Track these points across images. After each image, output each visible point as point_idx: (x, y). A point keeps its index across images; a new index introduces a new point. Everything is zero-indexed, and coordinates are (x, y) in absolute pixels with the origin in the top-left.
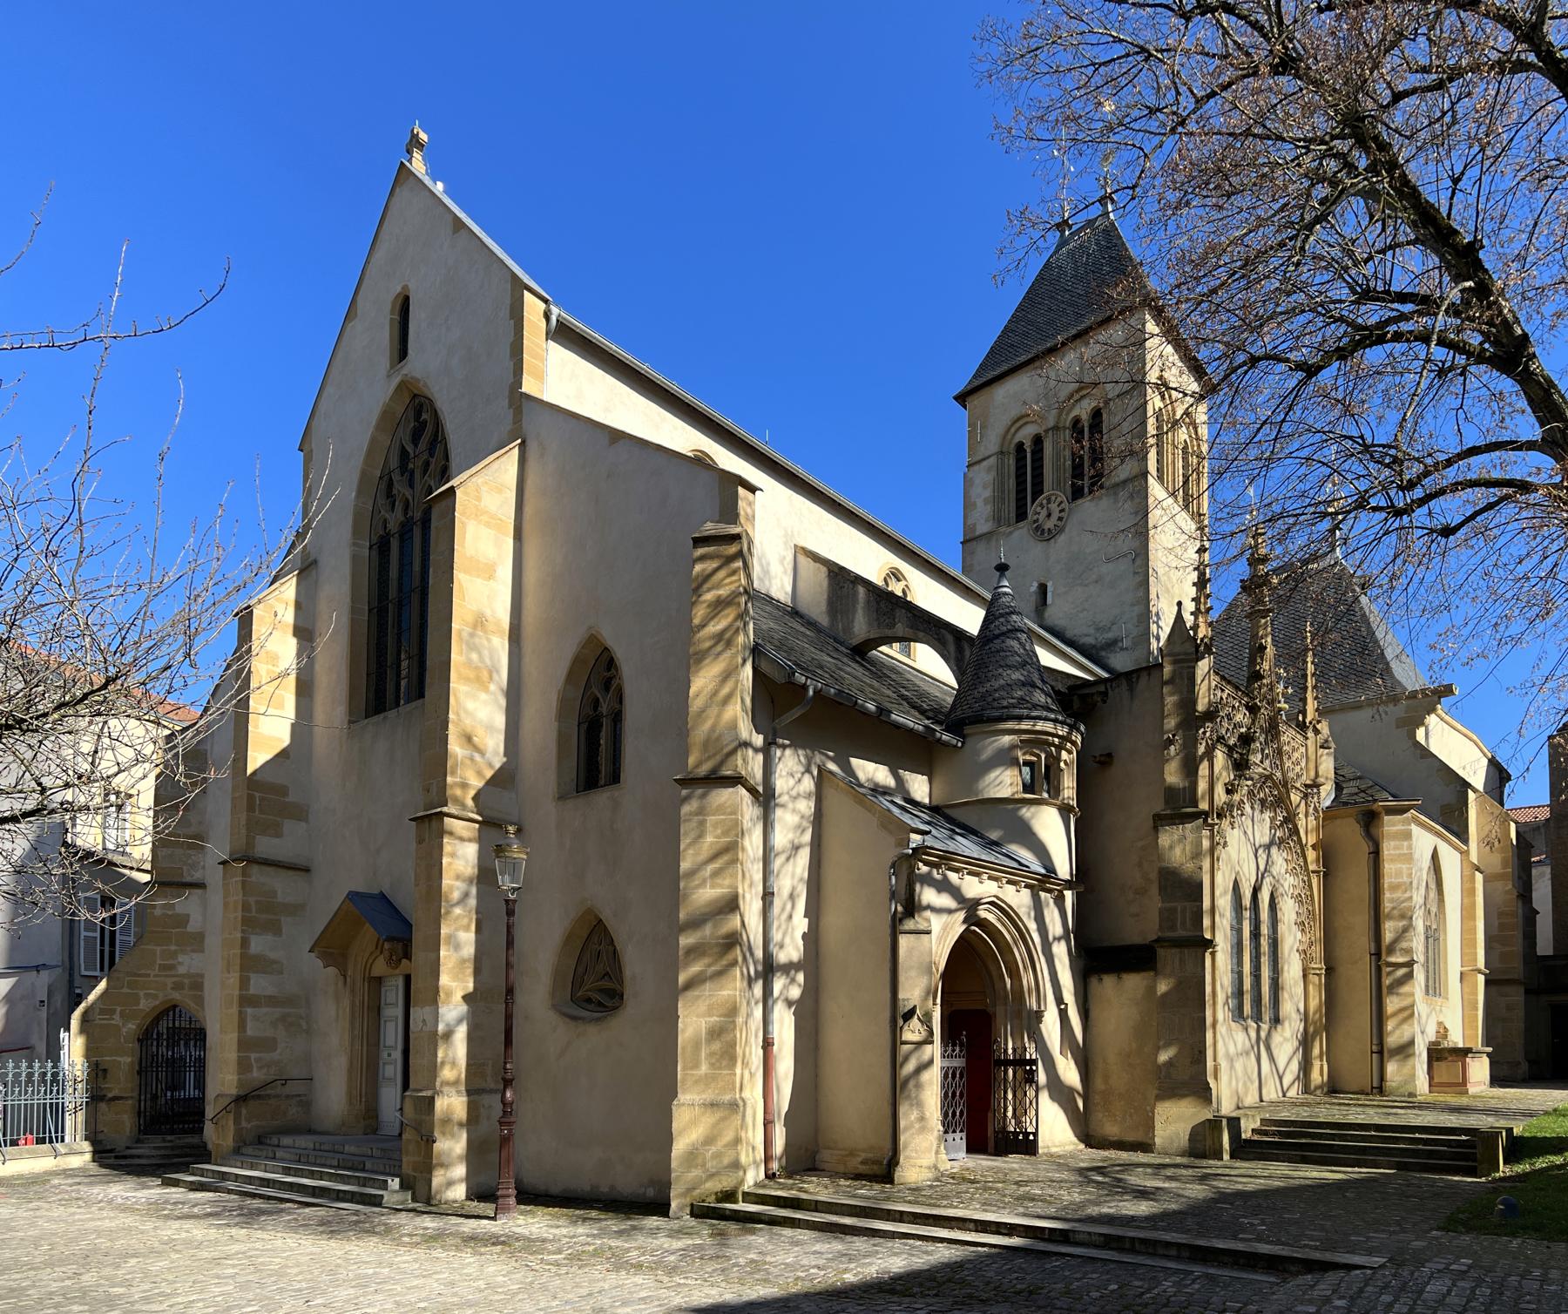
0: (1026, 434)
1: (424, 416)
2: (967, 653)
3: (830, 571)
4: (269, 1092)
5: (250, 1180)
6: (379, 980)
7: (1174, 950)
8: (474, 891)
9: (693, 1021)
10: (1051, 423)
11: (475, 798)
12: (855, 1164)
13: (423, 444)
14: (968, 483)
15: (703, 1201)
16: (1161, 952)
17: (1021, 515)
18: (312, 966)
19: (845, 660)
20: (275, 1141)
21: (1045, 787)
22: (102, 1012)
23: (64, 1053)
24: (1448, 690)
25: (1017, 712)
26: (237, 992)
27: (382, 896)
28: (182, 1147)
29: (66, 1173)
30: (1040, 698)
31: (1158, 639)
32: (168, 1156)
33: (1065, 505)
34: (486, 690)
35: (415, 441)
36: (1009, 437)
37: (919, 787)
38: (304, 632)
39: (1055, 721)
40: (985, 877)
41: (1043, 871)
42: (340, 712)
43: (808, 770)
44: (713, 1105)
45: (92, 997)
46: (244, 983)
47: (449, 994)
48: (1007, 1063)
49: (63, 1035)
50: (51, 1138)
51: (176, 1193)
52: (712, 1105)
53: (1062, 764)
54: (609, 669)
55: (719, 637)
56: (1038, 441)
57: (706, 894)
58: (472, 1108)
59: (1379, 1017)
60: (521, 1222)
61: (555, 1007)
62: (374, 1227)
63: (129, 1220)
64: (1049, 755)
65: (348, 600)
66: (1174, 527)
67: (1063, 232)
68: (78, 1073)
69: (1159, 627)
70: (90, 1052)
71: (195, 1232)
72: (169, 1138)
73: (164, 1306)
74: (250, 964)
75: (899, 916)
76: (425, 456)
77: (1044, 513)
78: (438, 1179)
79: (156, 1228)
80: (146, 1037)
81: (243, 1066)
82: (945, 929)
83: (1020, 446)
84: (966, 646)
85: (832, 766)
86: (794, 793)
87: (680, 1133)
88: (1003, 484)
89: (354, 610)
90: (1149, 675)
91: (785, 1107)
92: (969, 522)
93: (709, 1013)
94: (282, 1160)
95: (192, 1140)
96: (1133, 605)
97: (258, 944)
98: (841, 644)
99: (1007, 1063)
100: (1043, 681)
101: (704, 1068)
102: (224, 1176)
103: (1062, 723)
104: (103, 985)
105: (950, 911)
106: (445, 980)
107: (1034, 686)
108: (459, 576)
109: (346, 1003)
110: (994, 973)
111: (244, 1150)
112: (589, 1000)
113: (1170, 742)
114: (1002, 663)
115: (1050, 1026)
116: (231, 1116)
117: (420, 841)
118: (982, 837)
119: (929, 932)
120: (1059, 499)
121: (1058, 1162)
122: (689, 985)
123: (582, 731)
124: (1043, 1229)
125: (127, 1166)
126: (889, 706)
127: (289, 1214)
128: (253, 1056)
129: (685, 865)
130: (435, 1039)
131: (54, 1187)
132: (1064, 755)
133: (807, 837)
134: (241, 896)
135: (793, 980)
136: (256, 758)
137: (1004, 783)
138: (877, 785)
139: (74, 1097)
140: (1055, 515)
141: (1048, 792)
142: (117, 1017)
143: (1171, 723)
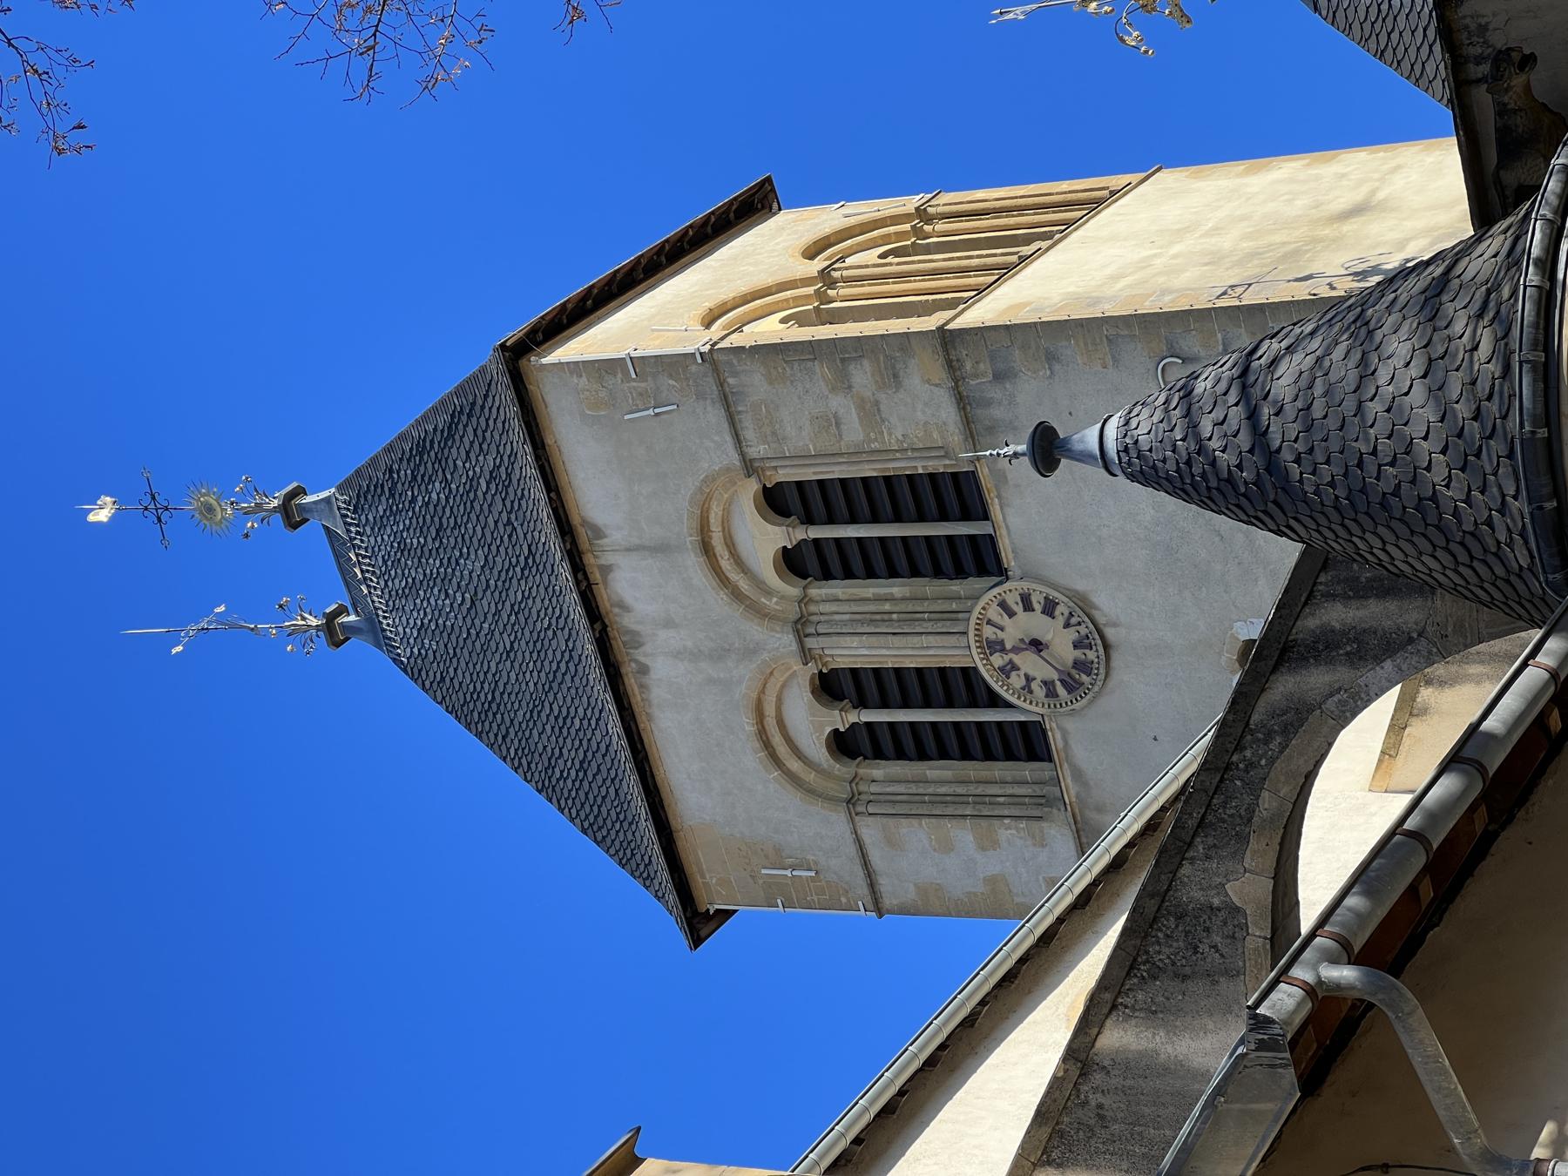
3: (1046, 1161)
10: (787, 641)
11: (853, 724)
25: (1527, 309)
33: (1010, 591)
36: (810, 777)
56: (830, 687)
67: (350, 630)
77: (1029, 663)
83: (843, 745)
88: (939, 799)
114: (1350, 405)
120: (994, 613)
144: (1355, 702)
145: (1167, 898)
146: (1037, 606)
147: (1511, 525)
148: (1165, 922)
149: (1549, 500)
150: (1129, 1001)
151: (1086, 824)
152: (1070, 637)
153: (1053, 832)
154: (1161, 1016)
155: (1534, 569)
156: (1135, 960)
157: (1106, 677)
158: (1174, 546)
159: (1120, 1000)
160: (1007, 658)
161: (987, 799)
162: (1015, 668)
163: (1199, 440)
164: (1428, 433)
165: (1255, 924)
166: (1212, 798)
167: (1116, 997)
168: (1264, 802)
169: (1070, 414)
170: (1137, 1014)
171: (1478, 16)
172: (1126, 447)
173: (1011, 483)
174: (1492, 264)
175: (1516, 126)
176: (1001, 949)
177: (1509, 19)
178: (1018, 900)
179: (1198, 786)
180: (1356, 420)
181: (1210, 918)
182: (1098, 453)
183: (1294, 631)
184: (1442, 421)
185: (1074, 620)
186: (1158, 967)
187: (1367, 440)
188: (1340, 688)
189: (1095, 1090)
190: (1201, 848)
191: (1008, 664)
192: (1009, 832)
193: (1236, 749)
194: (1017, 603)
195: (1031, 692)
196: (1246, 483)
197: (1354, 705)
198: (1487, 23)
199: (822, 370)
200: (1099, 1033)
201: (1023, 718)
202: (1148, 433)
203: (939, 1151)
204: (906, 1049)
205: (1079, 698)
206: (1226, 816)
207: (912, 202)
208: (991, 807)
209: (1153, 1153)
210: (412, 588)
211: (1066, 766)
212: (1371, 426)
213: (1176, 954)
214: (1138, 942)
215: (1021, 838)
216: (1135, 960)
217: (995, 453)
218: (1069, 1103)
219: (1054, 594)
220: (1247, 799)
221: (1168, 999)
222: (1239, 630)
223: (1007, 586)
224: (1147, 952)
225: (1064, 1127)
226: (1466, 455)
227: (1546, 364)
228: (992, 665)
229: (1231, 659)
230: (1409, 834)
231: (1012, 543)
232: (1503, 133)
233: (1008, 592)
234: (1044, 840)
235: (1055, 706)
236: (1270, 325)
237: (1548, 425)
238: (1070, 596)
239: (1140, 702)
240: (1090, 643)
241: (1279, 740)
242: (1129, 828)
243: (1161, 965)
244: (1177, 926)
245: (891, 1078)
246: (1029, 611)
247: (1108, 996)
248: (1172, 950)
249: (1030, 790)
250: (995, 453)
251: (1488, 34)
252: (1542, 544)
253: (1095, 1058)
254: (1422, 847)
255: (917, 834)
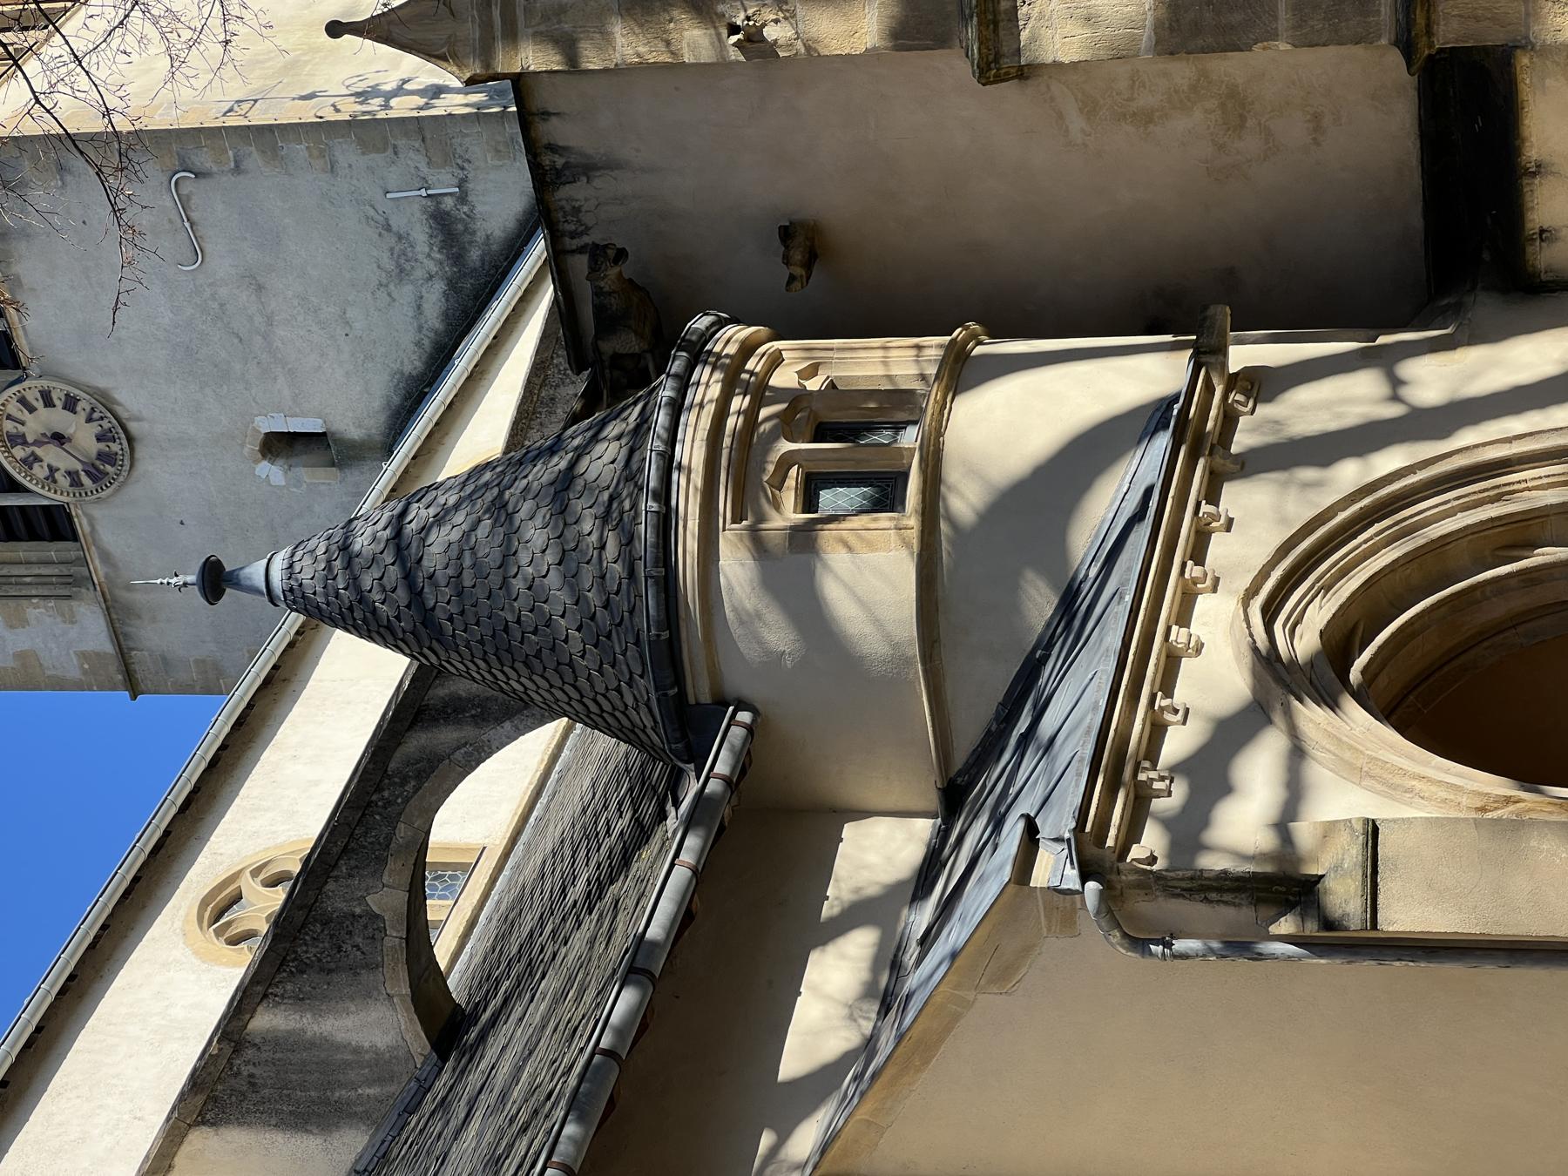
2: (462, 687)
3: (202, 1121)
16: (1449, 32)
19: (474, 1079)
21: (883, 437)
25: (645, 531)
30: (604, 460)
31: (437, 91)
39: (677, 408)
40: (1178, 635)
41: (1163, 441)
53: (813, 385)
66: (107, 53)
69: (399, 91)
75: (1311, 928)
82: (1361, 772)
84: (441, 692)
90: (546, 115)
92: (73, 672)
96: (332, 168)
98: (424, 1088)
100: (552, 451)
103: (684, 382)
105: (1297, 753)
107: (567, 478)
110: (1518, 602)
113: (753, 40)
114: (495, 580)
118: (1046, 644)
119: (1373, 831)
120: (14, 408)
126: (621, 941)
132: (784, 378)
138: (869, 991)
140: (58, 418)
141: (898, 427)
144: (479, 753)
145: (314, 908)
146: (57, 402)
147: (638, 696)
148: (312, 928)
149: (672, 688)
150: (279, 991)
151: (116, 601)
152: (94, 430)
153: (82, 610)
154: (308, 1001)
155: (657, 730)
156: (285, 958)
157: (132, 465)
158: (194, 347)
159: (270, 991)
160: (29, 450)
161: (13, 580)
162: (37, 459)
163: (359, 591)
164: (564, 612)
165: (393, 928)
166: (355, 829)
167: (267, 989)
168: (400, 833)
169: (84, 222)
170: (285, 1001)
171: (572, 200)
172: (291, 588)
173: (25, 287)
174: (611, 470)
175: (611, 305)
176: (116, 873)
177: (599, 205)
178: (48, 673)
179: (342, 821)
180: (501, 593)
181: (352, 924)
182: (265, 590)
183: (426, 698)
184: (576, 605)
185: (96, 415)
186: (306, 963)
187: (512, 610)
188: (466, 743)
189: (247, 1063)
190: (344, 869)
191: (30, 456)
192: (37, 610)
193: (375, 791)
194: (37, 400)
195: (55, 481)
196: (404, 632)
197: (478, 757)
198: (581, 206)
200: (251, 1017)
201: (46, 503)
202: (312, 579)
203: (79, 1083)
204: (39, 988)
205: (104, 488)
206: (366, 844)
208: (18, 587)
209: (299, 1110)
211: (93, 549)
212: (515, 600)
213: (322, 953)
214: (288, 945)
215: (50, 616)
216: (285, 958)
217: (165, 581)
218: (223, 1074)
219: (74, 391)
220: (386, 830)
221: (314, 988)
222: (261, 424)
223: (26, 384)
224: (295, 952)
225: (217, 1093)
226: (598, 636)
227: (666, 577)
228: (13, 457)
229: (254, 450)
230: (605, 1052)
231: (29, 343)
232: (599, 310)
233: (27, 390)
234: (74, 617)
235: (80, 494)
236: (280, 145)
237: (669, 628)
238: (91, 393)
239: (165, 490)
240: (114, 436)
241: (413, 783)
242: (220, 732)
243: (308, 961)
244: (322, 931)
246: (50, 406)
247: (259, 988)
248: (318, 950)
249: (56, 570)
250: (165, 581)
251: (580, 215)
252: (666, 722)
253: (247, 1037)
254: (615, 1064)
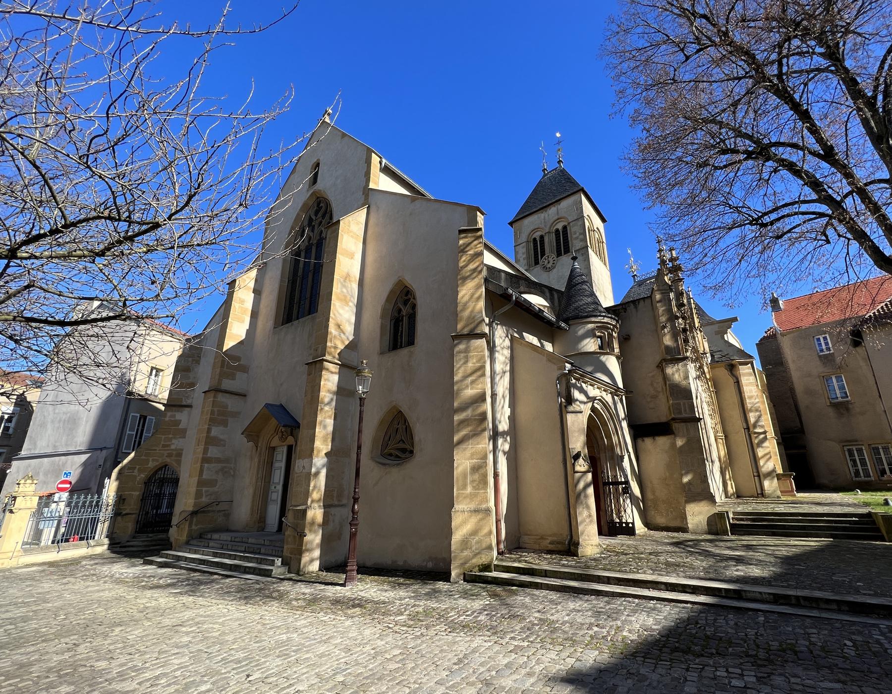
0: (537, 235)
1: (321, 205)
4: (209, 509)
5: (193, 560)
6: (274, 448)
7: (683, 424)
8: (335, 397)
9: (463, 461)
12: (546, 544)
13: (320, 215)
14: (516, 253)
15: (471, 571)
17: (537, 263)
18: (241, 442)
20: (209, 536)
22: (129, 468)
23: (105, 491)
24: (735, 319)
26: (201, 456)
27: (281, 406)
28: (156, 540)
29: (91, 557)
32: (149, 546)
34: (348, 305)
35: (316, 215)
37: (549, 347)
38: (257, 292)
39: (611, 318)
40: (596, 386)
42: (271, 324)
43: (507, 336)
44: (476, 511)
45: (125, 461)
46: (206, 451)
47: (319, 451)
48: (609, 484)
49: (107, 481)
50: (87, 537)
51: (151, 569)
52: (475, 511)
54: (406, 295)
55: (474, 270)
56: (542, 237)
57: (470, 392)
58: (326, 515)
59: (755, 459)
60: (361, 587)
61: (372, 458)
62: (271, 593)
63: (121, 591)
64: (609, 334)
65: (280, 277)
68: (110, 501)
70: (119, 490)
71: (161, 600)
72: (150, 535)
73: (134, 685)
74: (210, 441)
76: (321, 219)
77: (546, 262)
78: (305, 558)
79: (136, 597)
80: (148, 482)
81: (198, 495)
85: (516, 335)
86: (502, 346)
87: (457, 529)
89: (282, 281)
91: (505, 512)
93: (472, 457)
94: (212, 548)
95: (162, 536)
97: (215, 432)
99: (609, 484)
101: (469, 489)
102: (179, 558)
103: (614, 319)
104: (133, 455)
106: (318, 444)
108: (339, 256)
109: (256, 460)
110: (598, 437)
111: (191, 542)
112: (391, 455)
113: (664, 327)
115: (626, 464)
116: (187, 523)
117: (309, 374)
121: (643, 537)
122: (460, 442)
123: (392, 323)
124: (719, 589)
125: (125, 552)
127: (218, 583)
128: (204, 489)
129: (456, 378)
130: (308, 477)
131: (83, 566)
133: (508, 368)
134: (210, 408)
135: (506, 440)
136: (229, 344)
137: (591, 345)
139: (105, 515)
140: (551, 262)
142: (136, 471)
143: (663, 319)
199: (582, 231)
207: (604, 241)
210: (550, 180)
245: (495, 249)
255: (524, 250)
